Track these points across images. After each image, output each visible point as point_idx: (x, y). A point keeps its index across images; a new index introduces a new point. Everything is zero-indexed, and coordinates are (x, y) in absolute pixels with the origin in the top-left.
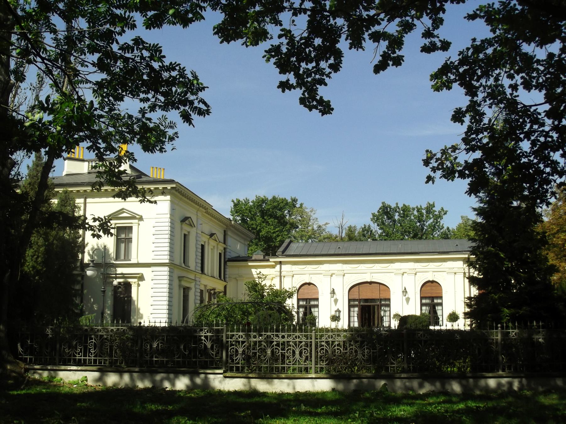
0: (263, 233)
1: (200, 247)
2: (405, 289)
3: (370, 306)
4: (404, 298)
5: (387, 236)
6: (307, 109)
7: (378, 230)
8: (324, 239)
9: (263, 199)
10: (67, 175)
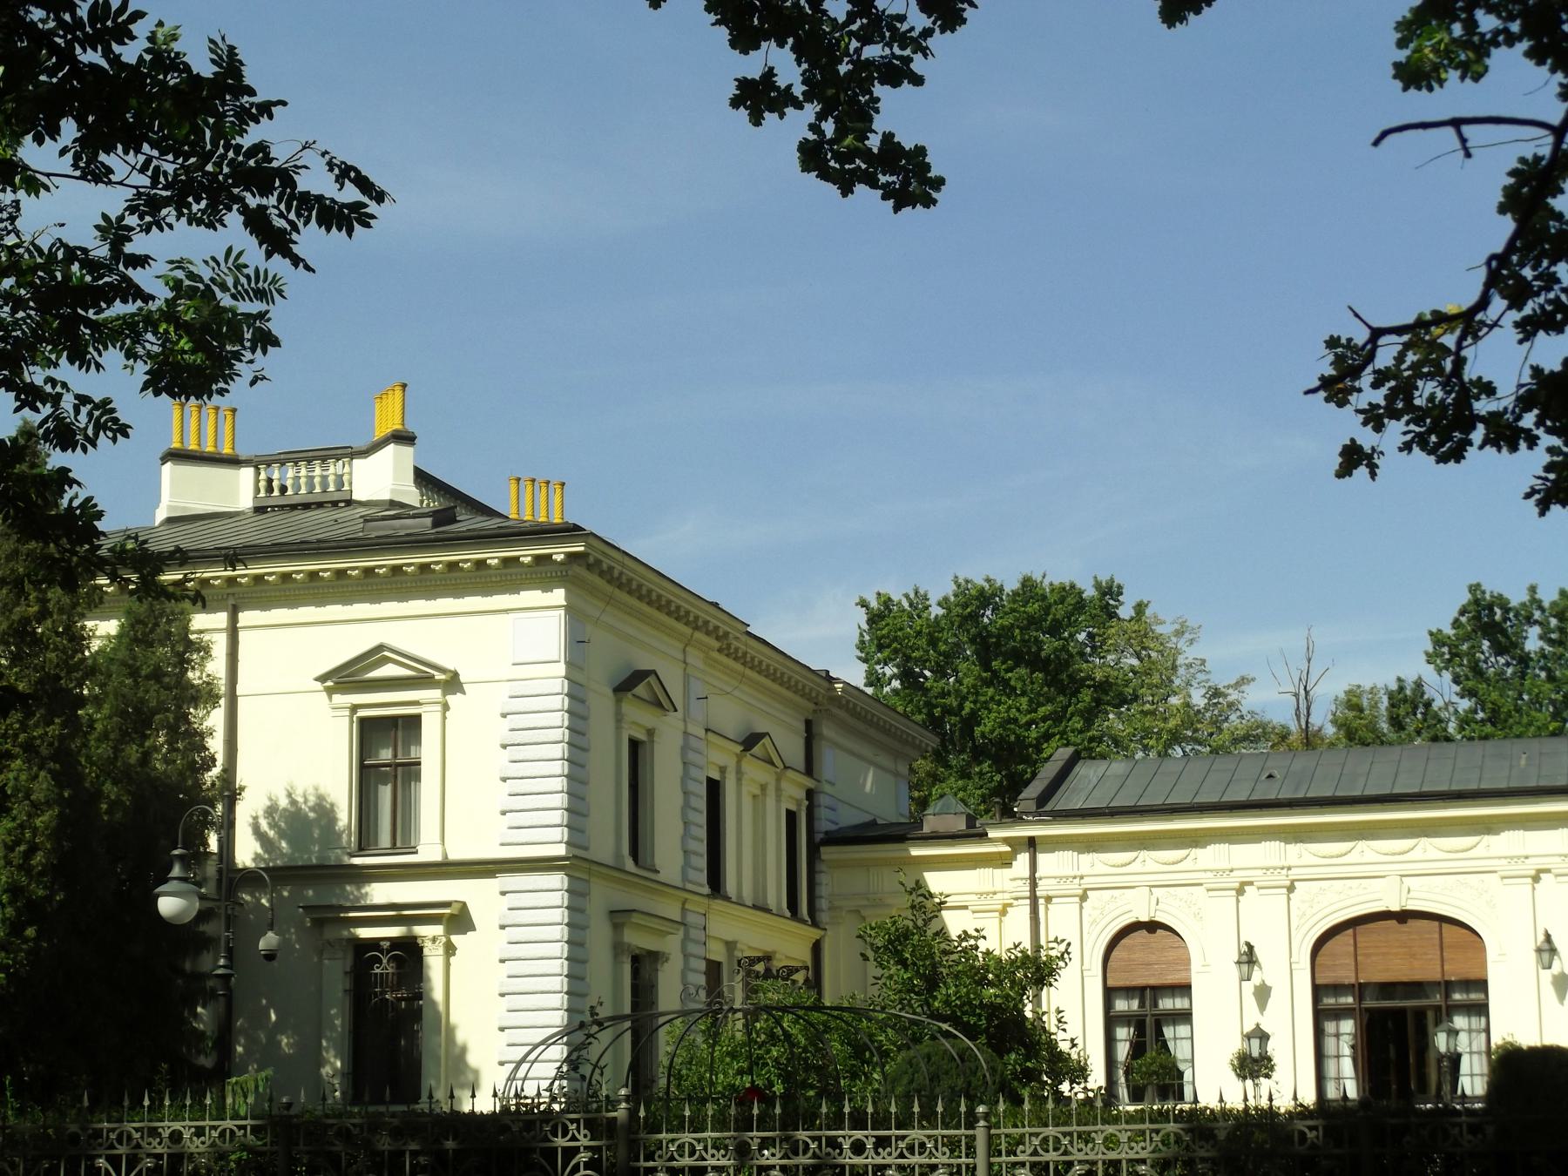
0: (987, 726)
1: (702, 790)
2: (1548, 938)
3: (1403, 1011)
4: (1547, 976)
5: (1495, 722)
6: (832, 190)
7: (1455, 699)
8: (1236, 741)
9: (982, 591)
10: (170, 521)
